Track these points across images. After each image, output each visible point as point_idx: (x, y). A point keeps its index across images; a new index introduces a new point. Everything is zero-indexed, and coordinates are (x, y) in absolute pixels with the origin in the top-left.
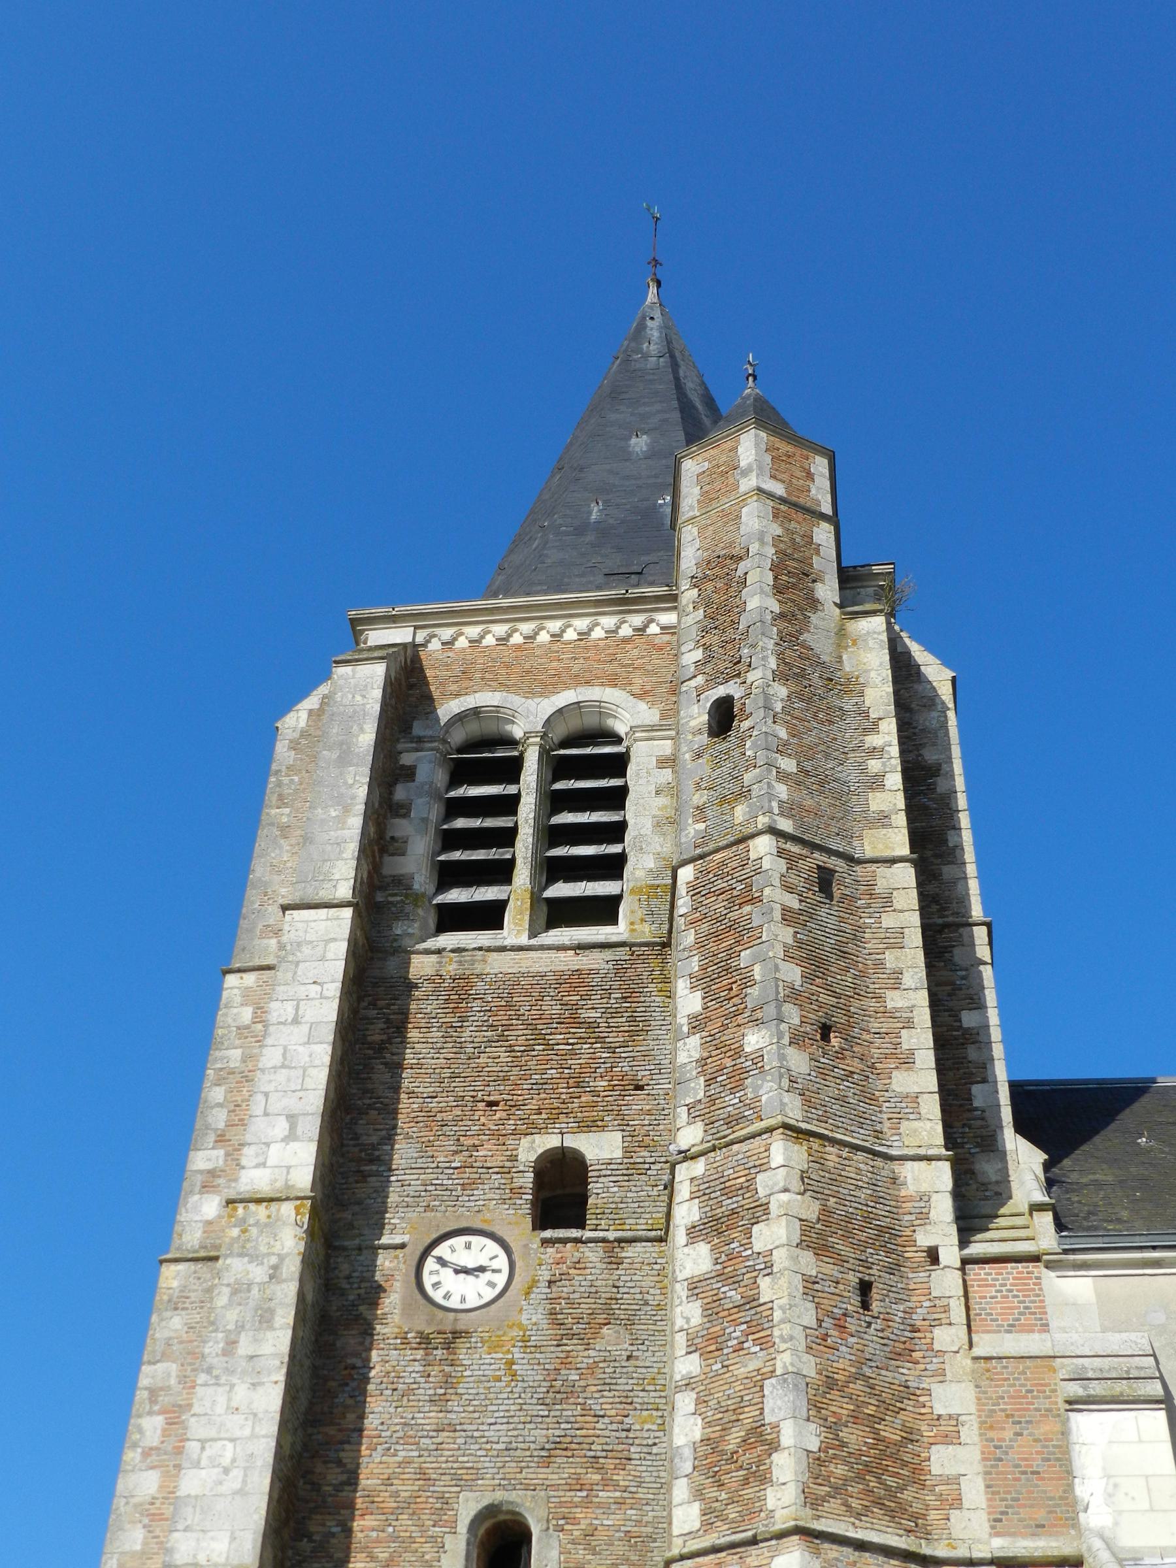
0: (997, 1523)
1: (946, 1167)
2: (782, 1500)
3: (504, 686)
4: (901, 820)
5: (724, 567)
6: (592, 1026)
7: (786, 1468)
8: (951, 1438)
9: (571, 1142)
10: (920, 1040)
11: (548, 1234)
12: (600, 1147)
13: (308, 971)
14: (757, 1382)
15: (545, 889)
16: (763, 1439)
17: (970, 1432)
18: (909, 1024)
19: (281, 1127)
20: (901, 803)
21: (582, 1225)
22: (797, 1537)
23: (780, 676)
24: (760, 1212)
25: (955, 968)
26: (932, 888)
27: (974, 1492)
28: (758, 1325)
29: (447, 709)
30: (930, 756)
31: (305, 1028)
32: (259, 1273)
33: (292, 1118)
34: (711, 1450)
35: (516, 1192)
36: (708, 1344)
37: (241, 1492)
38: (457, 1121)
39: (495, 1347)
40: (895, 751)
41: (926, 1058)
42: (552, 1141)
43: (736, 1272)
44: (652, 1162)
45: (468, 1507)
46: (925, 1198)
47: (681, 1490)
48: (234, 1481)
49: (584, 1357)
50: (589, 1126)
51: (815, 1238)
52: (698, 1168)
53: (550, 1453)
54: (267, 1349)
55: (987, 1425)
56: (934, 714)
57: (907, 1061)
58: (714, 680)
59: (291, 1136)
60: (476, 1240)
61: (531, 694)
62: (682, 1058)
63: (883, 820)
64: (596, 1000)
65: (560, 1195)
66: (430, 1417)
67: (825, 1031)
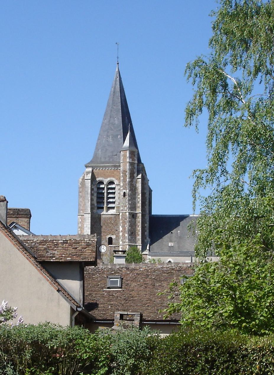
1: (141, 246)
4: (140, 207)
5: (124, 172)
6: (112, 223)
10: (140, 233)
11: (109, 246)
12: (114, 237)
13: (87, 221)
15: (108, 200)
20: (141, 237)
21: (112, 244)
25: (145, 219)
26: (144, 213)
29: (97, 179)
40: (141, 198)
41: (140, 235)
42: (109, 236)
44: (118, 237)
46: (139, 239)
52: (122, 246)
56: (146, 185)
58: (124, 189)
59: (88, 229)
61: (105, 178)
62: (120, 235)
63: (139, 198)
64: (113, 221)
67: (132, 233)
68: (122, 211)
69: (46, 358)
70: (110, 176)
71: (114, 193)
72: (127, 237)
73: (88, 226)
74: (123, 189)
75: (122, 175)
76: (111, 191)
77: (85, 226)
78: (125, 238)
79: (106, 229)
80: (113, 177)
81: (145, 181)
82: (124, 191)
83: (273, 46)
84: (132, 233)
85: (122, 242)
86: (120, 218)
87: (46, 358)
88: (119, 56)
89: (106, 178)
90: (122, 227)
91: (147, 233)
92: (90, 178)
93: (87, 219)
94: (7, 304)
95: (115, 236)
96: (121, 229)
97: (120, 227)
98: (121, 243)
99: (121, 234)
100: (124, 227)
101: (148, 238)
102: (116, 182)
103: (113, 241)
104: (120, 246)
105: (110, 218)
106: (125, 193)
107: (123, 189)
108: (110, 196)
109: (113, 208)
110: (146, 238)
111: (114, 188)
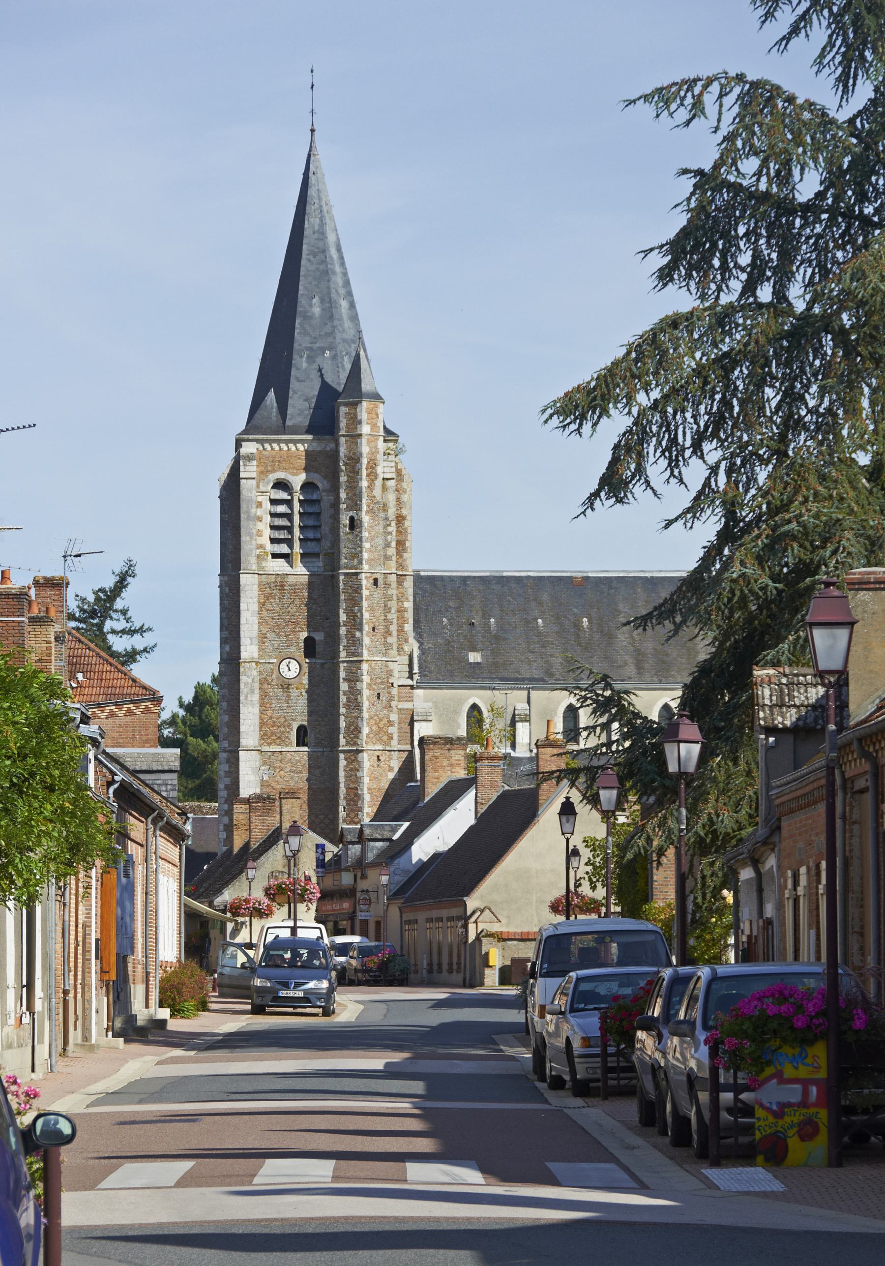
0: (399, 743)
3: (285, 470)
17: (396, 725)
18: (392, 623)
19: (249, 641)
22: (358, 853)
27: (396, 736)
30: (404, 512)
31: (250, 612)
32: (250, 681)
33: (251, 639)
34: (347, 727)
35: (300, 648)
36: (347, 706)
37: (254, 731)
39: (297, 689)
45: (295, 726)
47: (341, 736)
48: (252, 728)
51: (361, 809)
52: (345, 664)
54: (254, 699)
55: (399, 723)
58: (349, 509)
60: (298, 671)
62: (341, 632)
67: (374, 629)
68: (346, 568)
69: (853, 338)
72: (364, 636)
75: (343, 468)
78: (354, 641)
79: (298, 613)
82: (351, 513)
83: (832, 268)
84: (374, 629)
85: (347, 652)
88: (315, 127)
90: (345, 611)
91: (409, 627)
93: (247, 588)
94: (99, 705)
95: (322, 634)
96: (343, 617)
97: (341, 611)
98: (343, 654)
99: (343, 631)
100: (352, 611)
103: (319, 648)
106: (352, 519)
108: (284, 522)
110: (406, 641)
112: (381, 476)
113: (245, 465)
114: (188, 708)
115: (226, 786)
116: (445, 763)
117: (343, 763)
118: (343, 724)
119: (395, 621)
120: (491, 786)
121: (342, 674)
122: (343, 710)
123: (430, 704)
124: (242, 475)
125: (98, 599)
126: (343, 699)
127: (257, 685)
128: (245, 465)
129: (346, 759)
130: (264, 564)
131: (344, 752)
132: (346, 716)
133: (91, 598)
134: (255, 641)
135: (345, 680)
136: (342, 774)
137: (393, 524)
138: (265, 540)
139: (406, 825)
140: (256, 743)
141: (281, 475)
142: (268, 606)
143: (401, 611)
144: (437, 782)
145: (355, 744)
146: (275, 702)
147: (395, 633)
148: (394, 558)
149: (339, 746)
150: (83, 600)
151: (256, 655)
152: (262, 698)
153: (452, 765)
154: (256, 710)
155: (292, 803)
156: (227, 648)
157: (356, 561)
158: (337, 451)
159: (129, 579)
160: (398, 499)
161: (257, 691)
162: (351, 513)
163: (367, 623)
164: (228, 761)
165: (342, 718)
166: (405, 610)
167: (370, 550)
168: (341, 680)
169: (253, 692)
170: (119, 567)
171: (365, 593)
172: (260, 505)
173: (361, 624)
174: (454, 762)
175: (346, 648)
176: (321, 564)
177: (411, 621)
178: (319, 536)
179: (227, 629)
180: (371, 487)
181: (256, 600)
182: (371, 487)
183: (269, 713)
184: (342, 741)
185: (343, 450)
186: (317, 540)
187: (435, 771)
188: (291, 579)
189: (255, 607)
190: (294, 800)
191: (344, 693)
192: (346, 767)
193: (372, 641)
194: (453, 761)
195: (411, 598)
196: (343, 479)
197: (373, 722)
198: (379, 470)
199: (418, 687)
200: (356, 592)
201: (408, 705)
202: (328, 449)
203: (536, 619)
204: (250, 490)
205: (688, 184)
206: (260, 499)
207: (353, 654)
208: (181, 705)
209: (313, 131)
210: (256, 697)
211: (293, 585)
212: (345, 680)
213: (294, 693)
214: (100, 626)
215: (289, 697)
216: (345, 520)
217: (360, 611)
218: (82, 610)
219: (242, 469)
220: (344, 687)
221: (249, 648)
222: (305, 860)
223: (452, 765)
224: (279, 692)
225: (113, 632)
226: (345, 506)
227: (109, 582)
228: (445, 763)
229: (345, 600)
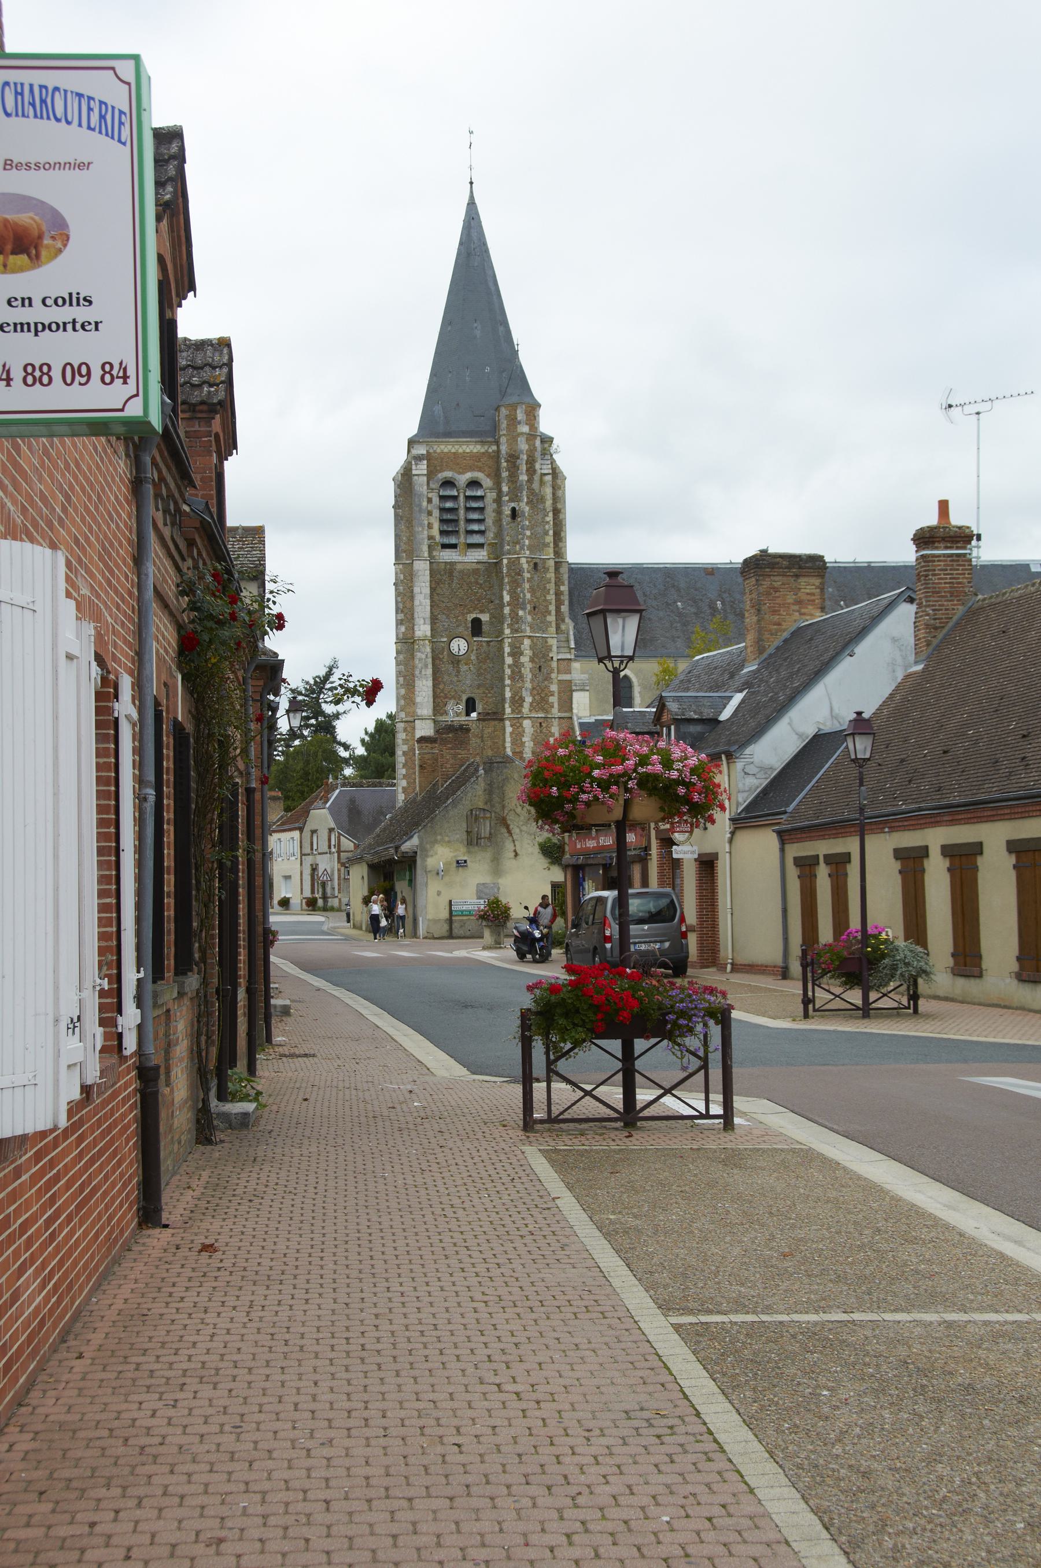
2: (526, 709)
3: (451, 470)
7: (526, 706)
8: (552, 695)
9: (479, 616)
12: (485, 617)
14: (521, 688)
16: (522, 700)
17: (556, 694)
19: (422, 621)
23: (527, 503)
24: (522, 654)
27: (556, 705)
28: (521, 677)
30: (559, 506)
32: (424, 656)
34: (512, 698)
36: (511, 678)
38: (829, 1486)
43: (517, 666)
45: (464, 698)
47: (507, 705)
49: (484, 667)
50: (482, 612)
51: (532, 660)
53: (479, 686)
57: (550, 613)
58: (511, 500)
61: (460, 473)
65: (477, 627)
66: (455, 679)
68: (509, 554)
69: (628, 970)
70: (471, 469)
71: (481, 510)
73: (424, 591)
74: (508, 501)
75: (505, 464)
76: (474, 505)
77: (416, 590)
80: (480, 470)
81: (559, 482)
82: (513, 505)
84: (534, 608)
86: (505, 570)
87: (628, 970)
89: (463, 473)
91: (565, 608)
92: (425, 472)
93: (420, 573)
96: (507, 598)
97: (505, 593)
98: (507, 631)
99: (507, 610)
101: (567, 620)
102: (487, 482)
103: (485, 628)
104: (506, 640)
105: (476, 572)
106: (514, 510)
107: (508, 501)
109: (480, 546)
110: (563, 621)
111: (482, 498)
112: (539, 471)
113: (416, 464)
114: (371, 735)
115: (404, 752)
116: (790, 599)
117: (509, 729)
118: (508, 694)
119: (554, 601)
120: (952, 594)
121: (507, 650)
122: (508, 682)
123: (586, 676)
124: (414, 472)
125: (316, 682)
126: (508, 671)
127: (430, 660)
128: (416, 464)
129: (512, 726)
130: (435, 553)
131: (510, 719)
132: (511, 687)
133: (312, 682)
134: (428, 621)
135: (509, 655)
136: (508, 739)
137: (551, 514)
138: (435, 532)
139: (738, 697)
140: (430, 712)
141: (448, 474)
142: (439, 591)
143: (558, 594)
144: (777, 631)
145: (520, 712)
146: (446, 677)
147: (553, 613)
148: (552, 545)
149: (504, 714)
150: (307, 683)
151: (429, 633)
152: (434, 673)
153: (799, 602)
154: (430, 683)
155: (495, 726)
156: (403, 629)
157: (518, 547)
158: (498, 451)
159: (334, 670)
160: (554, 494)
161: (430, 666)
162: (513, 505)
163: (529, 602)
164: (405, 730)
165: (507, 689)
166: (562, 593)
167: (529, 538)
168: (506, 655)
169: (426, 666)
170: (329, 662)
171: (527, 575)
172: (430, 500)
173: (524, 603)
174: (804, 597)
175: (510, 626)
176: (485, 553)
177: (567, 603)
178: (483, 528)
179: (402, 612)
180: (530, 481)
181: (428, 584)
182: (530, 481)
183: (441, 686)
184: (508, 710)
185: (504, 448)
186: (481, 532)
187: (775, 612)
188: (459, 567)
189: (427, 591)
190: (496, 722)
191: (509, 666)
192: (511, 733)
193: (533, 619)
194: (802, 595)
195: (566, 583)
196: (505, 474)
197: (535, 692)
198: (537, 466)
199: (575, 660)
200: (519, 575)
201: (567, 677)
202: (490, 450)
203: (675, 602)
204: (421, 485)
205: (165, 1217)
206: (430, 495)
207: (517, 631)
208: (366, 733)
209: (471, 183)
210: (429, 671)
211: (461, 572)
212: (509, 655)
213: (464, 668)
214: (318, 698)
215: (458, 672)
216: (507, 511)
217: (522, 592)
218: (306, 689)
219: (414, 467)
220: (509, 660)
221: (423, 627)
222: (511, 795)
223: (799, 602)
224: (450, 667)
225: (325, 702)
226: (507, 498)
227: (322, 672)
228: (790, 599)
229: (508, 583)
